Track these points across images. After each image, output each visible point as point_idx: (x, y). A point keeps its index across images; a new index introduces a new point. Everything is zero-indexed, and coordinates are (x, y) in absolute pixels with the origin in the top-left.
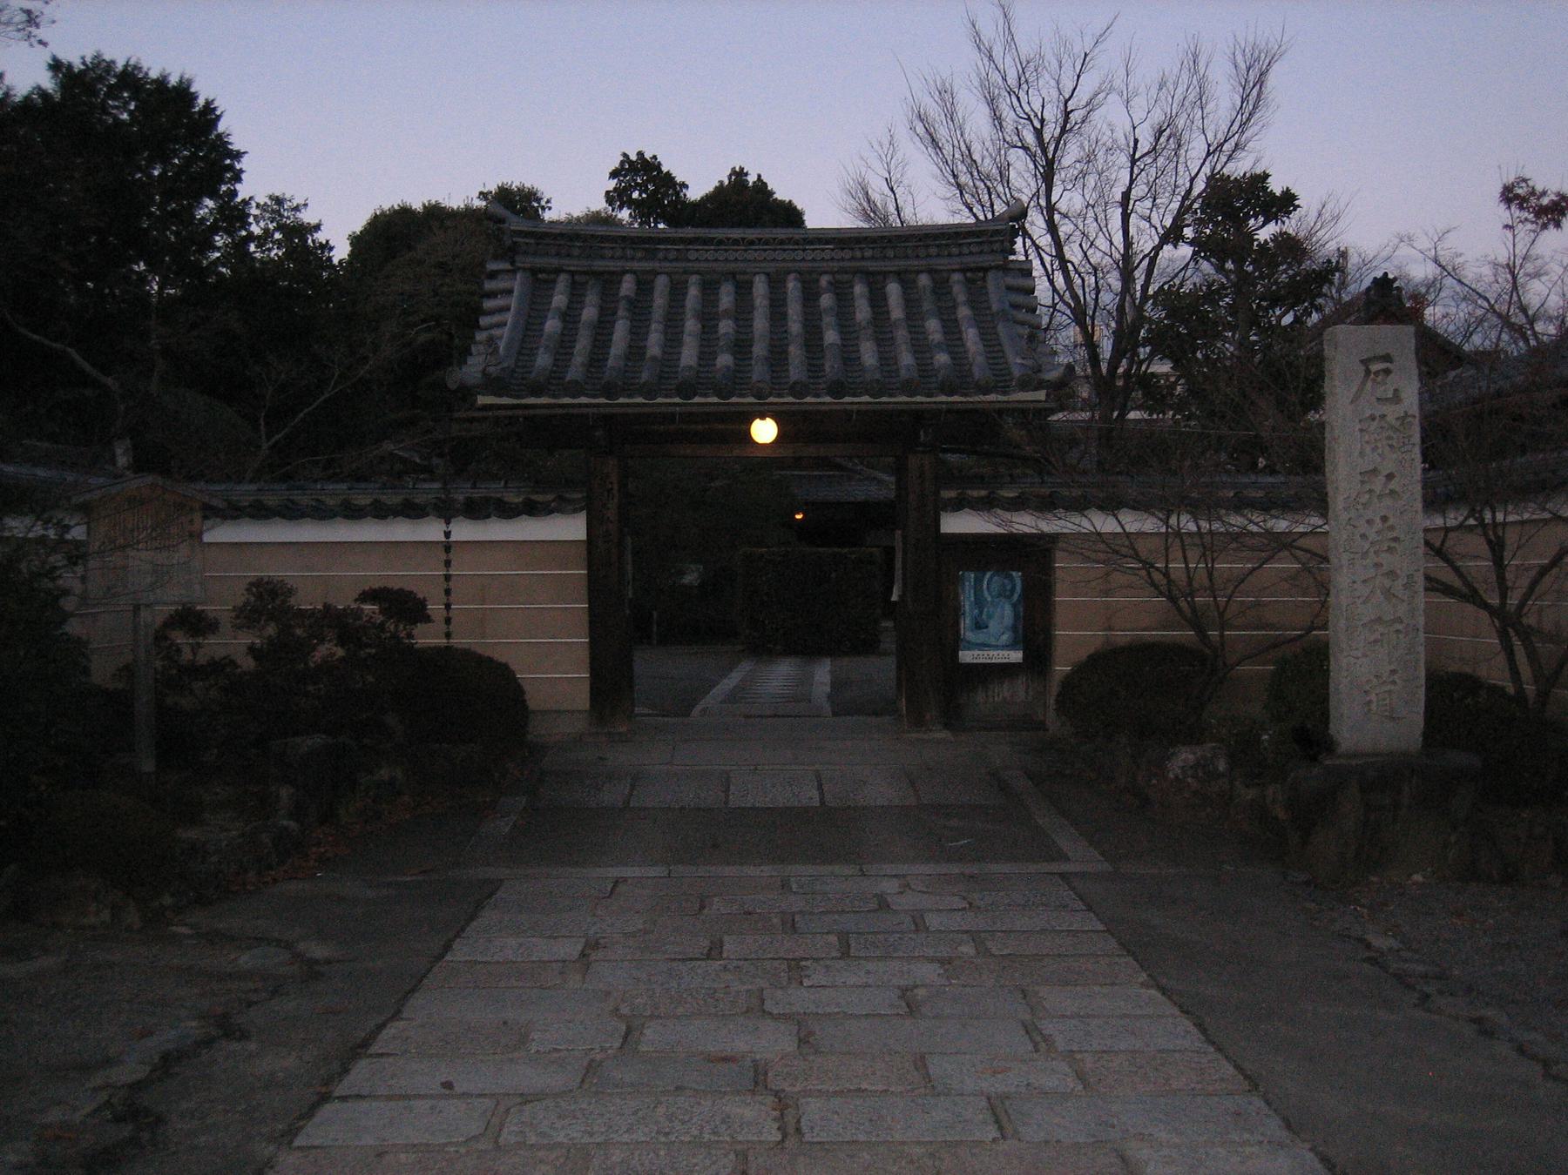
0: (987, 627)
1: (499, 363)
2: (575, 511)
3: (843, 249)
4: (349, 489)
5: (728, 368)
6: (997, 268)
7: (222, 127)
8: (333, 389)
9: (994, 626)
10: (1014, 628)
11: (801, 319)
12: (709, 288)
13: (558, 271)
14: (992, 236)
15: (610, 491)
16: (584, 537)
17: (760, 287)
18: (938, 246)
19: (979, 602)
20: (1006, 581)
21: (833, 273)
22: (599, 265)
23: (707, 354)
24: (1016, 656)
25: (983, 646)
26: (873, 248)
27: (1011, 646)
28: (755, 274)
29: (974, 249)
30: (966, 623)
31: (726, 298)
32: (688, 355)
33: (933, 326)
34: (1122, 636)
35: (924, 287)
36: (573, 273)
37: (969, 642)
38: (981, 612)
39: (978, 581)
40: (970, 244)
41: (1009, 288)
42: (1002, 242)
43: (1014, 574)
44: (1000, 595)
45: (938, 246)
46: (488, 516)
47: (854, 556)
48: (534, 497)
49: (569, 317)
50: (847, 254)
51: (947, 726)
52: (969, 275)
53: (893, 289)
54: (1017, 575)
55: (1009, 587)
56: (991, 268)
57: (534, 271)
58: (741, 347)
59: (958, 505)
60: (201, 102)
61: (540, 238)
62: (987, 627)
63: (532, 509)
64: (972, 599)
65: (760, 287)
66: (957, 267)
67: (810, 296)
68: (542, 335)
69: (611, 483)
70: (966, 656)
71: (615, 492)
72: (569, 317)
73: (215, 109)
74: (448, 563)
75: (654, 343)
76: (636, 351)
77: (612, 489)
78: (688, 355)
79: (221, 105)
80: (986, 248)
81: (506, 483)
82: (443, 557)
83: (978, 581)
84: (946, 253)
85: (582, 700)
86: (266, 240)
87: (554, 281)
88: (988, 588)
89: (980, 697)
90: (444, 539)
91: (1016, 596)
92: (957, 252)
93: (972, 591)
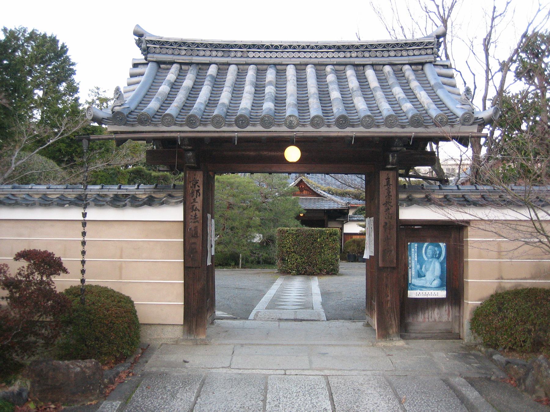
0: (425, 276)
1: (122, 105)
2: (177, 203)
3: (339, 52)
4: (48, 188)
5: (270, 109)
6: (431, 62)
7: (68, 54)
8: (60, 136)
9: (429, 276)
10: (441, 277)
11: (315, 86)
12: (261, 73)
13: (172, 63)
14: (426, 45)
15: (198, 191)
16: (183, 220)
17: (291, 71)
18: (395, 51)
19: (421, 261)
20: (436, 249)
21: (333, 65)
22: (196, 59)
23: (257, 102)
24: (442, 294)
25: (422, 287)
26: (357, 52)
27: (439, 287)
28: (287, 65)
29: (416, 53)
30: (412, 272)
31: (271, 75)
32: (246, 103)
33: (398, 91)
34: (509, 284)
35: (388, 72)
36: (181, 64)
37: (414, 285)
38: (421, 268)
39: (419, 249)
40: (413, 50)
41: (440, 75)
42: (432, 49)
43: (441, 244)
44: (432, 257)
45: (395, 51)
46: (125, 206)
47: (328, 232)
48: (153, 195)
49: (175, 86)
50: (342, 55)
51: (402, 337)
52: (413, 67)
53: (370, 73)
54: (443, 245)
55: (438, 252)
56: (426, 63)
57: (159, 63)
58: (280, 101)
59: (410, 202)
60: (60, 45)
61: (163, 45)
62: (425, 276)
63: (150, 202)
64: (416, 259)
65: (291, 71)
66: (407, 62)
67: (321, 77)
68: (157, 92)
69: (199, 187)
70: (412, 294)
71: (201, 191)
72: (175, 86)
73: (66, 46)
74: (84, 234)
75: (225, 97)
76: (212, 102)
77: (199, 190)
78: (246, 103)
79: (68, 45)
80: (423, 52)
81: (138, 186)
82: (81, 229)
83: (419, 249)
84: (400, 55)
85: (178, 317)
86: (93, 103)
87: (169, 69)
88: (426, 253)
89: (420, 318)
90: (82, 219)
91: (442, 258)
92: (406, 55)
93: (416, 254)
